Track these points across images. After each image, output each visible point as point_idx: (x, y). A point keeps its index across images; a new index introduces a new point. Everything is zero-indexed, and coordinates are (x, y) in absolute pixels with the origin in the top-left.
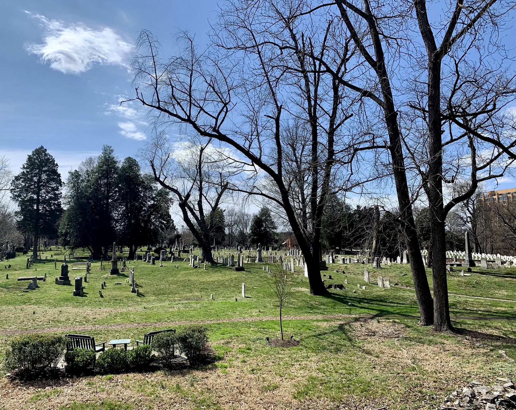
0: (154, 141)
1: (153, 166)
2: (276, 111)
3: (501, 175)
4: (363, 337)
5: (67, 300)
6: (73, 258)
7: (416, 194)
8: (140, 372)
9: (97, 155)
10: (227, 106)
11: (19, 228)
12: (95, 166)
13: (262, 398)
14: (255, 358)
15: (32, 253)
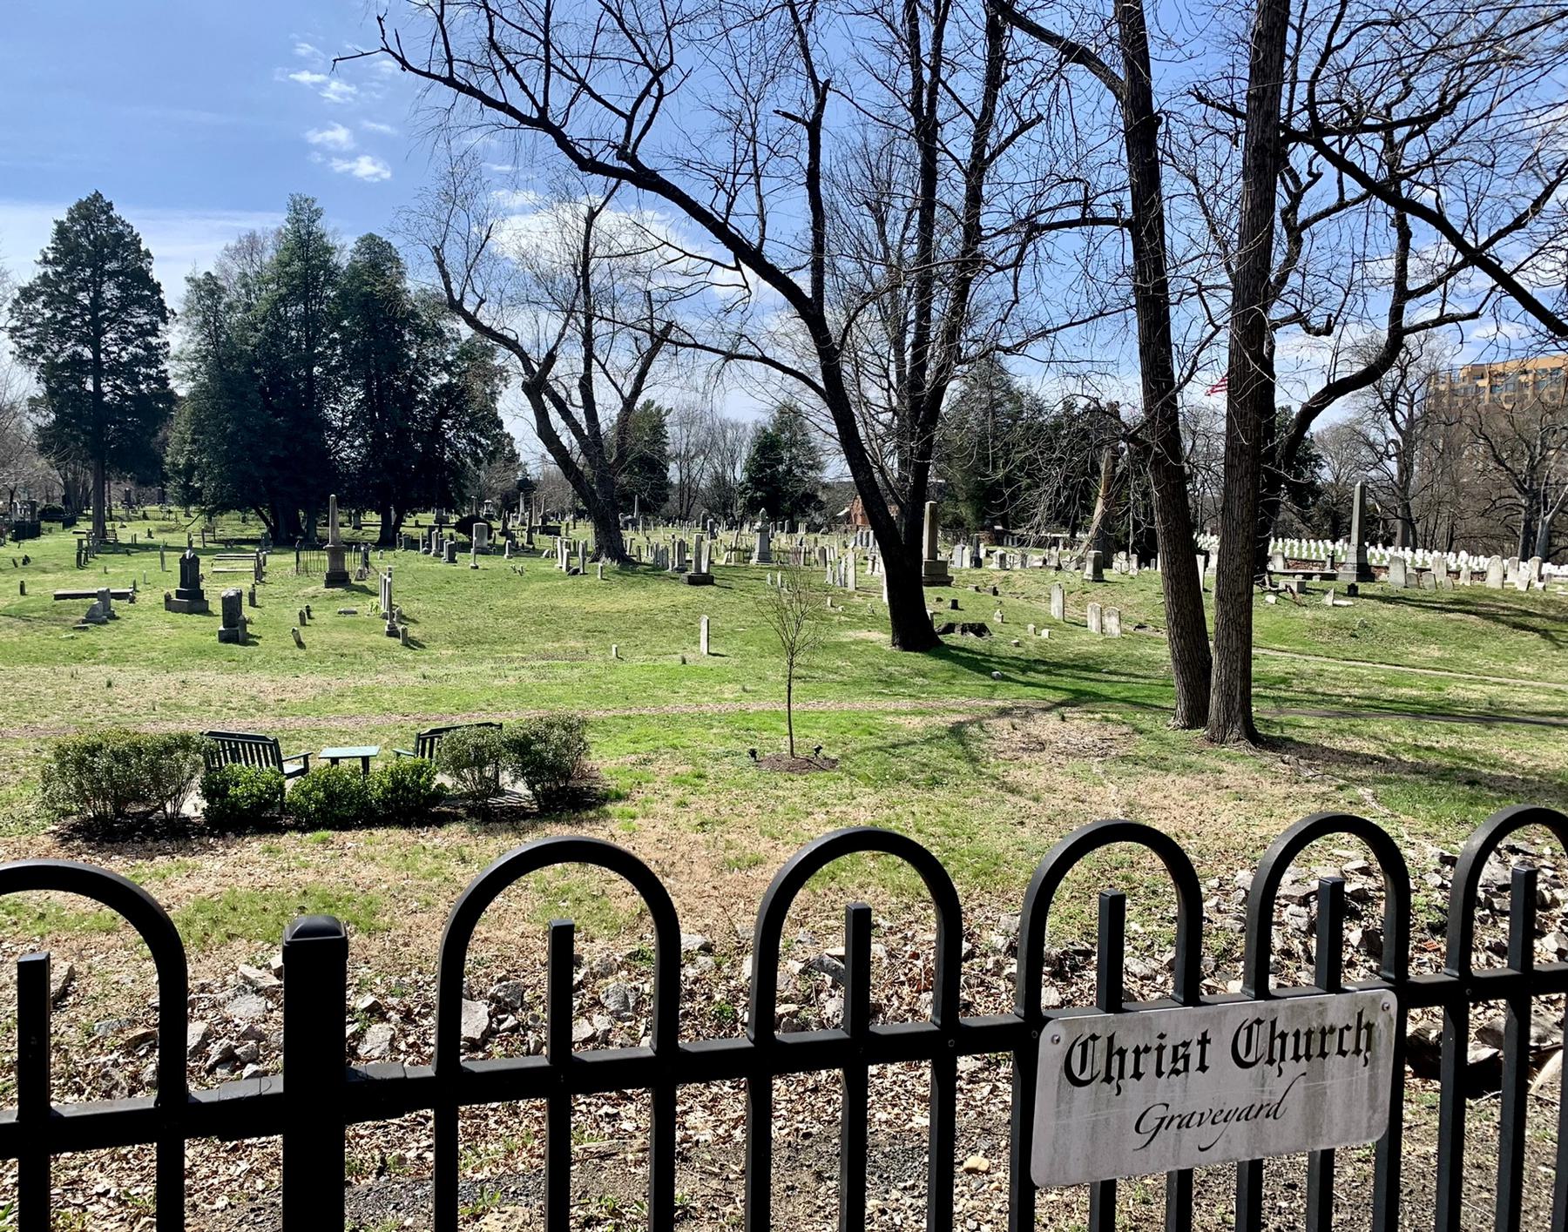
0: (443, 182)
1: (441, 264)
2: (812, 101)
3: (1475, 315)
4: (1010, 754)
5: (201, 653)
6: (215, 542)
7: (1189, 364)
8: (406, 824)
9: (272, 224)
10: (664, 78)
11: (43, 449)
12: (266, 260)
13: (717, 884)
14: (713, 796)
15: (90, 525)
